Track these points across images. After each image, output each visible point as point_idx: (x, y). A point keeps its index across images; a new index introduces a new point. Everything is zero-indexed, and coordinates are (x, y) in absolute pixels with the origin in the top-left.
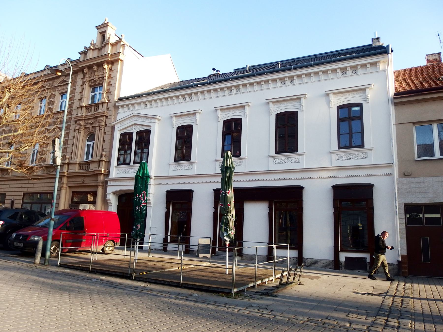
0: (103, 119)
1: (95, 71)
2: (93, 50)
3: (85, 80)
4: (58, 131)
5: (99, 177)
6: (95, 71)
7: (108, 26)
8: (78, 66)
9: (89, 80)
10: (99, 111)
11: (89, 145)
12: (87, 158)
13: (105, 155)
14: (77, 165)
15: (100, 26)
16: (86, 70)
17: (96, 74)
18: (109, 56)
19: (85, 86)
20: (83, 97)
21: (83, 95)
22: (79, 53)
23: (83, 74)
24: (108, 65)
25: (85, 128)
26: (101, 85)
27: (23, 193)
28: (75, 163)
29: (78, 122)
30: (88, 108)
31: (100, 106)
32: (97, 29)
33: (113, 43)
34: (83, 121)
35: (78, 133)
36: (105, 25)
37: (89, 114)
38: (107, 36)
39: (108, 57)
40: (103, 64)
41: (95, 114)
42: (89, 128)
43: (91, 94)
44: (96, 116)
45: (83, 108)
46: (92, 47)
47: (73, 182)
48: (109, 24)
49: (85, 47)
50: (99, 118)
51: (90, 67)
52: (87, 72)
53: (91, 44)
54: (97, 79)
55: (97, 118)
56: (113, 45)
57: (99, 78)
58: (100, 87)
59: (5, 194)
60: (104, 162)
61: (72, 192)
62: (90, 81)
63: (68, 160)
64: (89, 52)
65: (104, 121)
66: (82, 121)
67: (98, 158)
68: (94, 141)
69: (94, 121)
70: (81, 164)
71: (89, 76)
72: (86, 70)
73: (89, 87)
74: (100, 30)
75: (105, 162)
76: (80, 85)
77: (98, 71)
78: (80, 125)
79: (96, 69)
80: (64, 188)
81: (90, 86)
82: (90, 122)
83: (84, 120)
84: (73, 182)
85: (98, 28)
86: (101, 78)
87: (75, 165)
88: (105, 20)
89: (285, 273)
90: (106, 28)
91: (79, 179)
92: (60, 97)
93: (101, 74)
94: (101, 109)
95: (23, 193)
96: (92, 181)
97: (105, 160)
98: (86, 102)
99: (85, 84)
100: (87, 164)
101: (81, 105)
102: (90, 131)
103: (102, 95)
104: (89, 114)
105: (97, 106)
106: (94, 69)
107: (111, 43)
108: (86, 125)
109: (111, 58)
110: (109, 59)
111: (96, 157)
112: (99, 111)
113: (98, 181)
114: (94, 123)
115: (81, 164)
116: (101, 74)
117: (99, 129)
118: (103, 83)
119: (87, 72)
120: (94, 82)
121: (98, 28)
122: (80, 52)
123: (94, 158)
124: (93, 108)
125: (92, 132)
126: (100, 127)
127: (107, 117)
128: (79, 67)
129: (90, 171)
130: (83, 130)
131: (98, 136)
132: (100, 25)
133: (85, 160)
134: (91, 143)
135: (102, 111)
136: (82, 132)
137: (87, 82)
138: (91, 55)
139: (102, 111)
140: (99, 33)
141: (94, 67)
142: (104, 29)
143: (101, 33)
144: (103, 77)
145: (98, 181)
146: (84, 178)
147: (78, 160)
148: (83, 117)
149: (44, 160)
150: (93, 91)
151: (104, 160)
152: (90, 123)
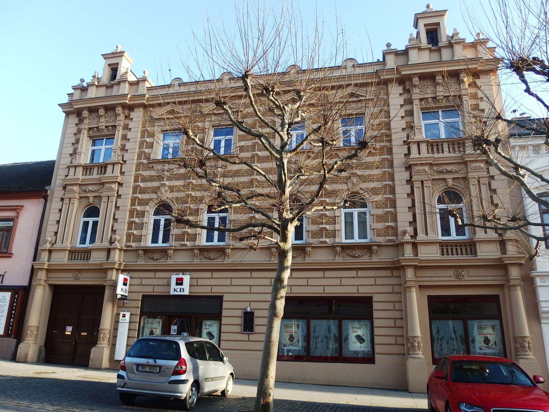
0: (115, 186)
1: (102, 116)
2: (97, 86)
3: (82, 126)
4: (166, 191)
5: (109, 273)
6: (102, 116)
7: (122, 56)
8: (73, 105)
9: (89, 128)
10: (69, 176)
11: (86, 224)
12: (83, 241)
13: (119, 241)
14: (67, 252)
15: (420, 15)
16: (85, 113)
17: (102, 120)
18: (128, 97)
19: (83, 136)
20: (78, 151)
21: (79, 149)
22: (72, 87)
23: (78, 118)
24: (123, 110)
25: (80, 197)
26: (110, 137)
27: (142, 295)
28: (64, 250)
29: (69, 188)
30: (87, 169)
31: (110, 168)
32: (105, 58)
33: (132, 82)
34: (78, 186)
35: (107, 202)
36: (120, 54)
37: (87, 177)
38: (122, 70)
39: (127, 99)
40: (116, 109)
41: (101, 179)
42: (445, 179)
43: (91, 148)
44: (102, 181)
45: (78, 169)
46: (96, 83)
47: (432, 277)
48: (125, 54)
49: (81, 80)
50: (107, 185)
51: (93, 110)
52: (87, 115)
53: (94, 77)
54: (104, 127)
55: (103, 184)
56: (131, 84)
57: (106, 127)
58: (106, 139)
59: (221, 297)
60: (117, 252)
61: (499, 295)
62: (90, 129)
63: (49, 243)
64: (90, 89)
65: (116, 189)
66: (76, 187)
67: (106, 244)
68: (98, 217)
69: (98, 188)
70: (73, 253)
71: (90, 121)
72: (85, 113)
73: (88, 137)
74: (108, 61)
75: (120, 250)
76: (73, 134)
77: (105, 117)
78: (73, 191)
79: (103, 114)
80: (42, 287)
81: (90, 137)
82: (90, 189)
83: (80, 185)
84: (432, 277)
85: (106, 56)
86: (110, 127)
87: (64, 253)
88: (117, 48)
89: (301, 409)
90: (119, 59)
91: (69, 275)
92: (90, 143)
93: (93, 122)
94: (111, 172)
95: (141, 294)
96: (490, 276)
97: (120, 248)
98: (84, 159)
99: (82, 132)
100: (87, 253)
101: (75, 163)
102: (89, 202)
103: (113, 153)
104: (87, 177)
105: (103, 167)
106: (100, 113)
107: (129, 80)
108: (82, 192)
109: (129, 101)
110: (127, 102)
111: (102, 242)
112: (107, 175)
113: (106, 278)
114: (97, 191)
115: (76, 252)
116: (93, 122)
117: (107, 200)
118: (115, 134)
119: (87, 115)
120: (97, 131)
121: (106, 56)
122: (74, 86)
123: (97, 244)
124: (96, 169)
125: (94, 203)
126: (70, 199)
127: (120, 184)
128: (75, 108)
129: (90, 262)
130: (78, 200)
131: (66, 213)
132: (419, 14)
133: (79, 246)
134: (91, 220)
135: (73, 178)
136: (76, 203)
137: (86, 130)
138: (92, 93)
139: (113, 175)
140: (107, 65)
141: (100, 111)
142: (439, 19)
143: (109, 65)
144: (115, 127)
145: (107, 279)
146: (463, 271)
147: (69, 246)
148: (79, 181)
149: (139, 239)
150: (94, 144)
151: (118, 247)
152: (448, 172)
